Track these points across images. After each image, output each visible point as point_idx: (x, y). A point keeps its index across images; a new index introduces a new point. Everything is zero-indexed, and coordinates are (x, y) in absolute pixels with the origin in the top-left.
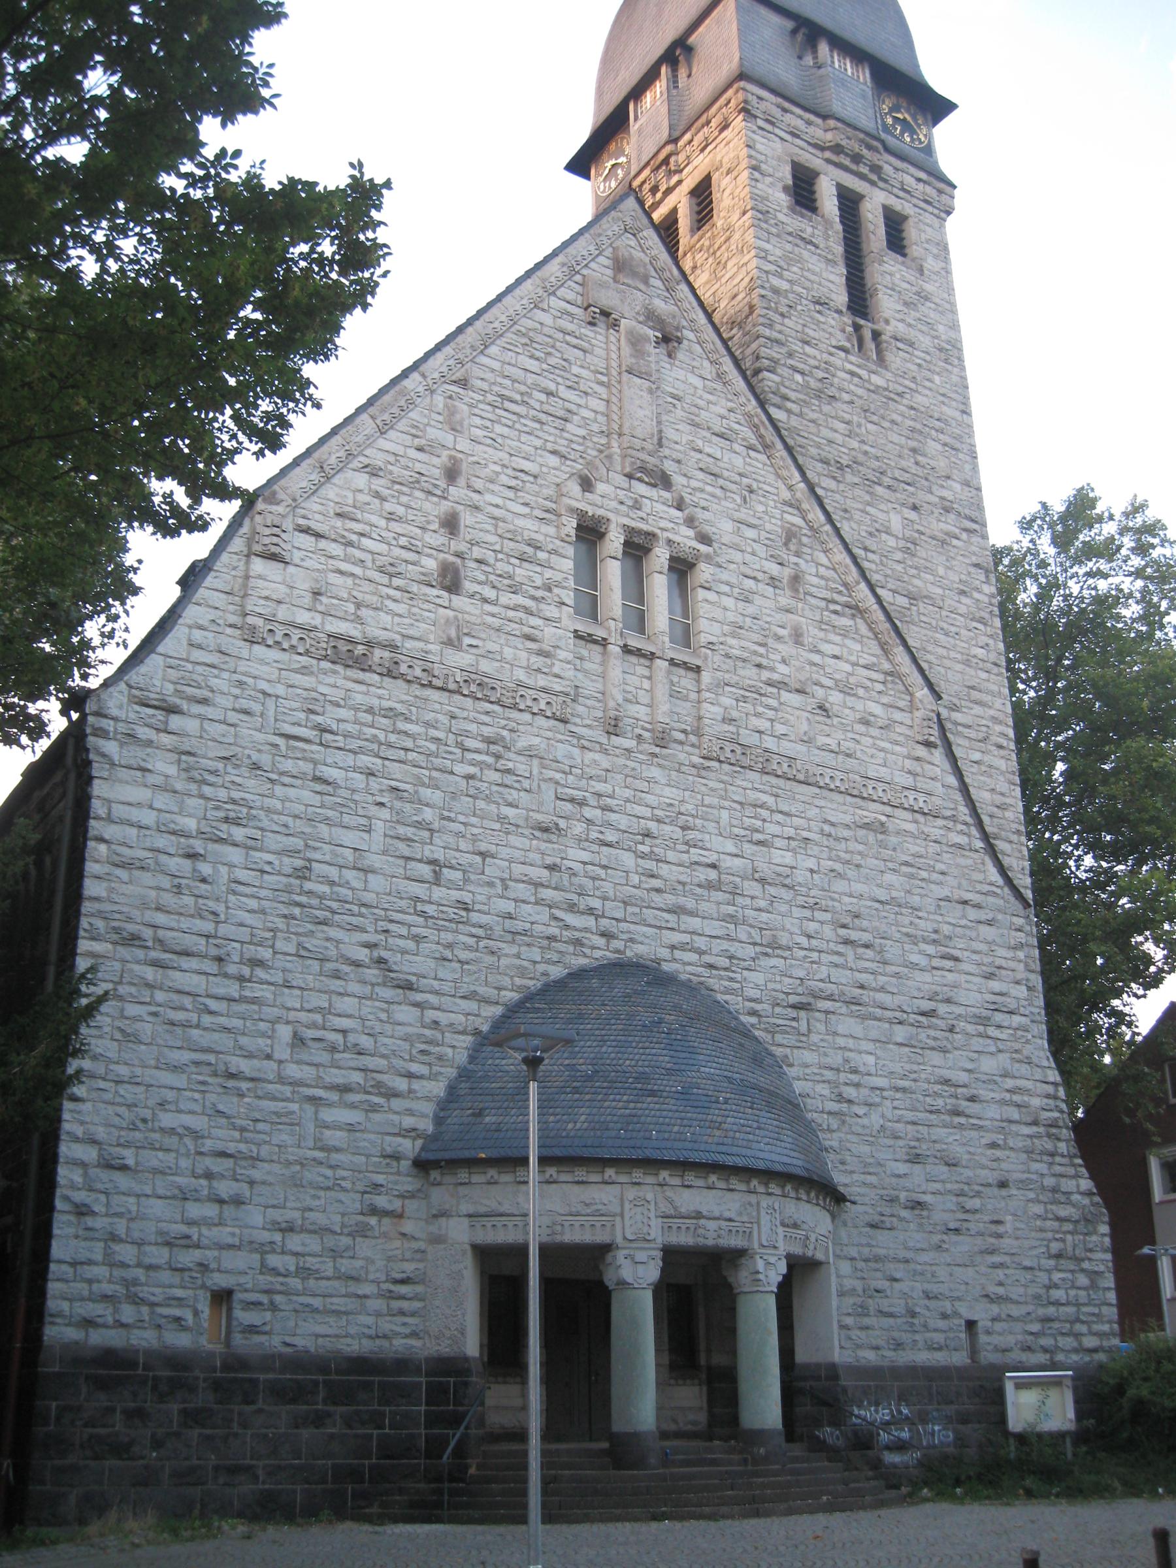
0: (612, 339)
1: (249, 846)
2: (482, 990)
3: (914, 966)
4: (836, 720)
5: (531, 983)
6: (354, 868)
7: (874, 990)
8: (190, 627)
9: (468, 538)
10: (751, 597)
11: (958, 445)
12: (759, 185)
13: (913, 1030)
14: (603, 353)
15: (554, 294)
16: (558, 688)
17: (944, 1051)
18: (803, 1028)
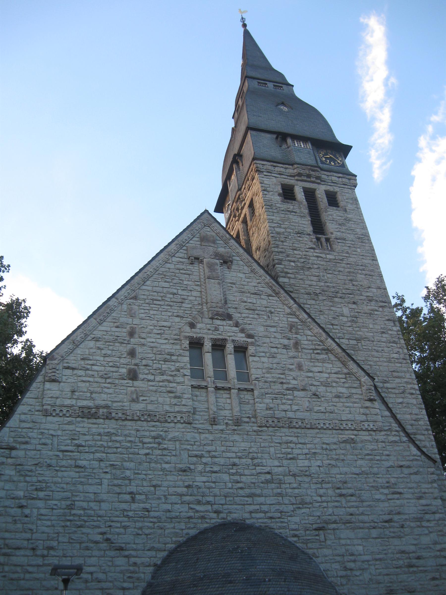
0: (201, 267)
1: (46, 499)
2: (156, 545)
3: (378, 500)
4: (323, 399)
5: (181, 539)
6: (95, 501)
7: (358, 515)
8: (20, 414)
9: (140, 357)
10: (275, 355)
11: (373, 274)
12: (267, 196)
13: (382, 530)
14: (198, 274)
15: (174, 256)
16: (185, 410)
17: (400, 537)
18: (322, 538)
